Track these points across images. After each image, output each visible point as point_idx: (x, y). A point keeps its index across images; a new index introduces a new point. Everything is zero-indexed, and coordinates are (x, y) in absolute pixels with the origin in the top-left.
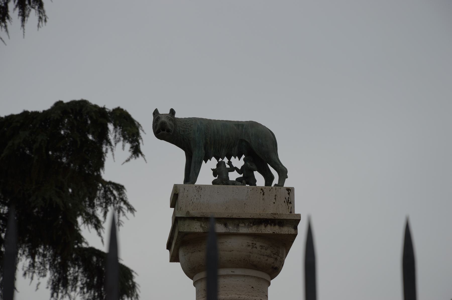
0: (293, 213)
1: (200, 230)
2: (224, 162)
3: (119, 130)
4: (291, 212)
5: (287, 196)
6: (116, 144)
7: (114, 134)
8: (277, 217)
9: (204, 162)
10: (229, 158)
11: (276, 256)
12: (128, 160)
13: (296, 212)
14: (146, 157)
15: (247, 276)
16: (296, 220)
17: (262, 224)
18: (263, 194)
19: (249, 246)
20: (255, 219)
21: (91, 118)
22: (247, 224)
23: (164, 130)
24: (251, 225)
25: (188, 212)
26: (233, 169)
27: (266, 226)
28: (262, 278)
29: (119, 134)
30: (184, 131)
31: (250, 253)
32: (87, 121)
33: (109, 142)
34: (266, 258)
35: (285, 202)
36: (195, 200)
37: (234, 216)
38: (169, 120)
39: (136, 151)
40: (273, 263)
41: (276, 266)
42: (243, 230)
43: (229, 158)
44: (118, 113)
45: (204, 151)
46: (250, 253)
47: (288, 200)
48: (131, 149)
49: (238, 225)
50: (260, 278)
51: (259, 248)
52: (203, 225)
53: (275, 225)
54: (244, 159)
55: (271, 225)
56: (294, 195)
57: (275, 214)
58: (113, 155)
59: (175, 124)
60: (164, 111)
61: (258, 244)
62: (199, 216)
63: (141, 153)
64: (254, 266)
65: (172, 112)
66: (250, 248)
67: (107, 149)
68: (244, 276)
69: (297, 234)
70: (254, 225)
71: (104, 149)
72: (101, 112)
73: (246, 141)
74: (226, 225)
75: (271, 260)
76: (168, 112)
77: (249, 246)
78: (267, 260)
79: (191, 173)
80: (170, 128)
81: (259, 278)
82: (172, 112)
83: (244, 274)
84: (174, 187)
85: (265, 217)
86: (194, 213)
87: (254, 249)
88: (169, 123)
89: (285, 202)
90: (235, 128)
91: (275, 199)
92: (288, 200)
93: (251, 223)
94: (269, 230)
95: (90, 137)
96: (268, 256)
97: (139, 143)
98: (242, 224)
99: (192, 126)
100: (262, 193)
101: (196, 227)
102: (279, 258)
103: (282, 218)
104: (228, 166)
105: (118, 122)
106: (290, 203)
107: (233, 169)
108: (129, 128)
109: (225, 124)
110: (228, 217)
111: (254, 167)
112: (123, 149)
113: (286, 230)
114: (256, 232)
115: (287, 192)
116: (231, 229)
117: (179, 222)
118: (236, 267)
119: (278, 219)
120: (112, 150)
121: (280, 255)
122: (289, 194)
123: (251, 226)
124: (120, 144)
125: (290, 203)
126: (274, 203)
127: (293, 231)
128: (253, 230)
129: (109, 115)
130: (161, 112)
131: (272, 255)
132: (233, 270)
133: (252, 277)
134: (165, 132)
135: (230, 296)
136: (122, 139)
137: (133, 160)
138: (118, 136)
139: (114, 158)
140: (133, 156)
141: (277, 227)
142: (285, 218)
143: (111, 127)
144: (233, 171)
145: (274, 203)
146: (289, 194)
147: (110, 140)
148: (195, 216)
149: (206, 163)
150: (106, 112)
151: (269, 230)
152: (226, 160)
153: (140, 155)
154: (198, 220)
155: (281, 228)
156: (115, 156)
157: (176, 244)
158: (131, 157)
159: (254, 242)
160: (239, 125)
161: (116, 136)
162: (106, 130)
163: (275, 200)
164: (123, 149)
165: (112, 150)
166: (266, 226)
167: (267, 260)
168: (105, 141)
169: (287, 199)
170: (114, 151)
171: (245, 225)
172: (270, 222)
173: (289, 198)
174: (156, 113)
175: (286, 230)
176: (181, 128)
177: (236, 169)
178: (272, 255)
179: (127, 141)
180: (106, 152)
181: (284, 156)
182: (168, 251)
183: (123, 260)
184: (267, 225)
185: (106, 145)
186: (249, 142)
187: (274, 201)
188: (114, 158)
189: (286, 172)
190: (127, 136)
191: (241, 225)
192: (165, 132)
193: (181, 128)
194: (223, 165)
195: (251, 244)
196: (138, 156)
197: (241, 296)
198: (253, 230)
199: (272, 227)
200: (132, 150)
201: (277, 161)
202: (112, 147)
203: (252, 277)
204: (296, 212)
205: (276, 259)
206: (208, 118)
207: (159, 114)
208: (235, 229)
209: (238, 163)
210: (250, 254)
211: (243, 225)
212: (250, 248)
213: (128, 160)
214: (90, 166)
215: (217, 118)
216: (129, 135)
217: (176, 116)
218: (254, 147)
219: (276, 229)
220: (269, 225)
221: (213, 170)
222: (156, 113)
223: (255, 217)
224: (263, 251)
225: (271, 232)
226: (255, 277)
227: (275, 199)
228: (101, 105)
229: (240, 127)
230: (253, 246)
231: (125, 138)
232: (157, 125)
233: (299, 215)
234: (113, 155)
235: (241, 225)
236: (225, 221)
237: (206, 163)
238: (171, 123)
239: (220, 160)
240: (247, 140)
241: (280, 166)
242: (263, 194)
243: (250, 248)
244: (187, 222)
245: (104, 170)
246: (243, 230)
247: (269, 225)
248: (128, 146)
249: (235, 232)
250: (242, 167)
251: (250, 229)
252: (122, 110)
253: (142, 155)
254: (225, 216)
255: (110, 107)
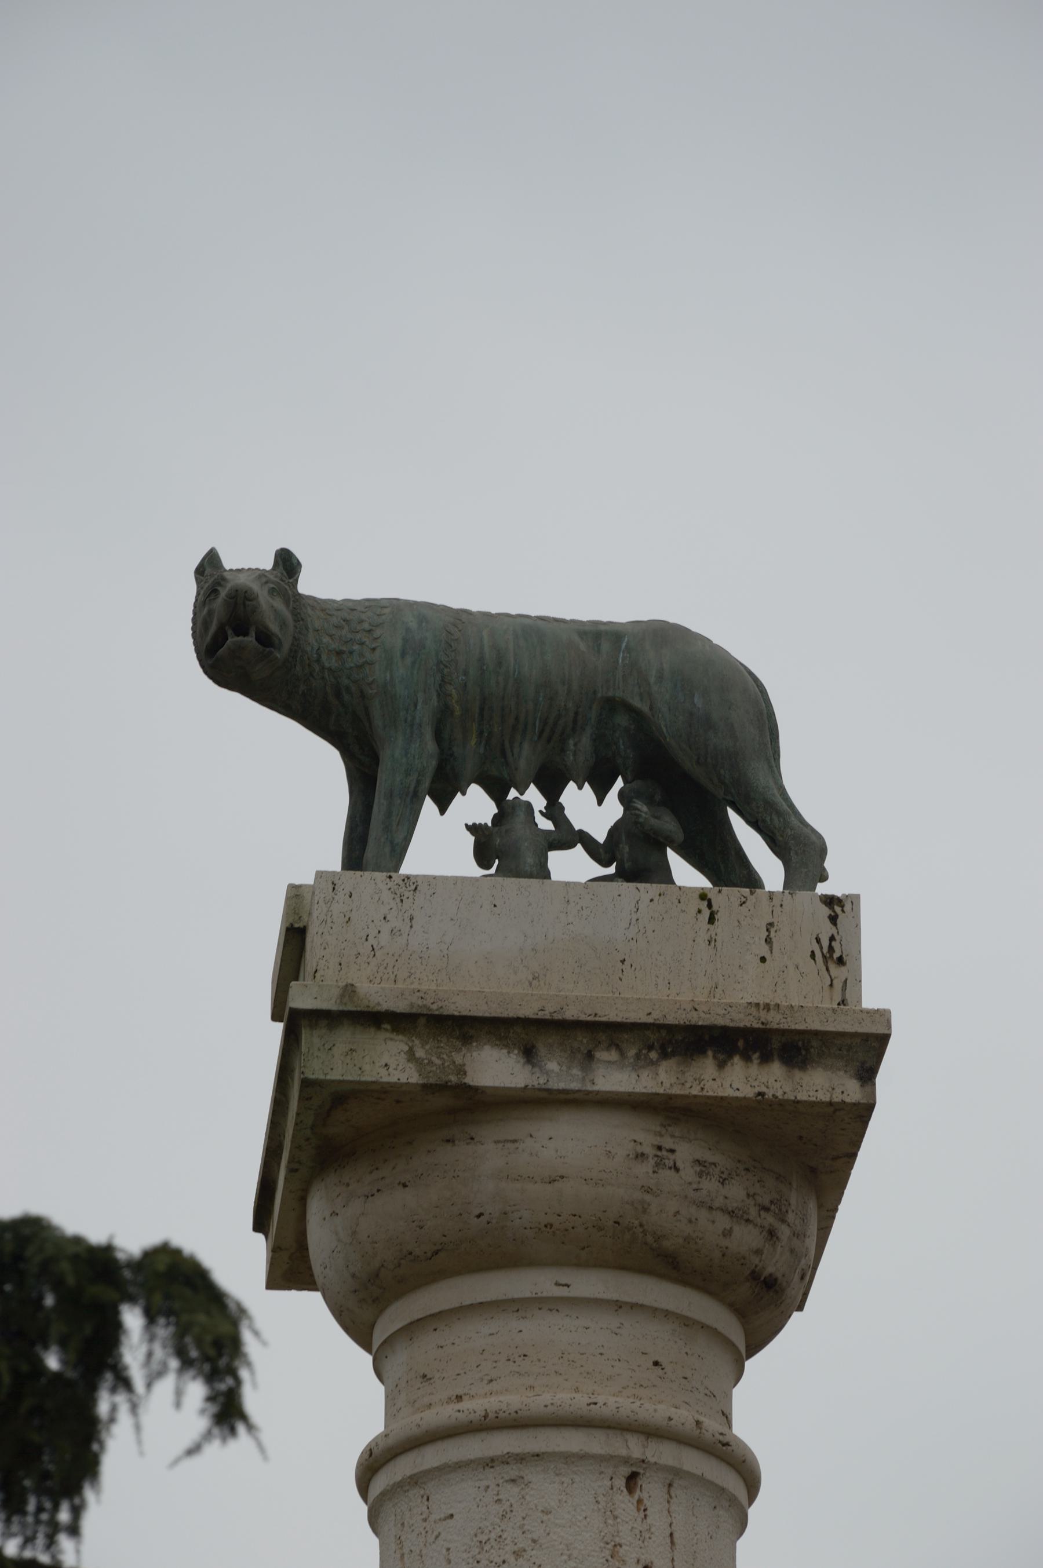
0: (851, 1006)
1: (406, 1074)
2: (529, 806)
3: (163, 1331)
4: (843, 1002)
5: (826, 930)
6: (149, 1385)
7: (143, 1349)
8: (775, 1020)
9: (429, 806)
10: (552, 793)
11: (769, 1219)
12: (194, 1450)
13: (870, 1000)
14: (265, 1436)
15: (633, 1306)
16: (866, 1037)
17: (702, 1052)
18: (712, 920)
19: (641, 1156)
20: (670, 1028)
21: (58, 1286)
22: (632, 1052)
23: (241, 630)
24: (653, 1055)
25: (349, 990)
26: (567, 837)
27: (721, 1065)
28: (703, 1326)
29: (164, 1347)
30: (339, 653)
31: (648, 1190)
32: (41, 1298)
33: (124, 1382)
34: (723, 1222)
35: (813, 955)
36: (385, 937)
37: (571, 1013)
38: (272, 592)
39: (228, 1413)
40: (758, 1252)
41: (770, 1270)
42: (614, 1077)
43: (552, 793)
44: (161, 1266)
45: (431, 746)
46: (648, 1190)
47: (831, 949)
48: (208, 1405)
49: (590, 1056)
50: (695, 1322)
51: (688, 1173)
52: (420, 1053)
53: (766, 1059)
54: (622, 796)
55: (747, 1058)
56: (858, 926)
57: (767, 1007)
58: (138, 1428)
59: (297, 616)
60: (247, 555)
61: (686, 1152)
62: (400, 1006)
63: (243, 1417)
64: (670, 1263)
65: (287, 564)
66: (647, 1167)
67: (114, 1409)
68: (618, 1306)
69: (870, 1107)
70: (665, 1055)
71: (103, 1408)
72: (100, 1261)
73: (629, 709)
74: (529, 1054)
75: (746, 1238)
76: (267, 563)
77: (641, 1156)
78: (727, 1233)
79: (373, 836)
80: (274, 627)
81: (687, 1322)
82: (287, 564)
83: (615, 1296)
84: (288, 899)
85: (720, 1022)
86: (379, 993)
87: (667, 1174)
88: (269, 607)
89: (813, 955)
90: (582, 646)
91: (768, 941)
92: (831, 949)
93: (650, 1048)
94: (738, 1080)
95: (53, 1362)
96: (731, 1214)
97: (238, 1382)
98: (608, 1049)
99: (378, 632)
100: (706, 913)
101: (389, 1062)
102: (784, 1232)
103: (802, 1027)
104: (545, 824)
105: (158, 1298)
106: (841, 961)
107: (567, 837)
108: (201, 1318)
109: (535, 631)
110: (541, 1015)
111: (668, 824)
112: (178, 1404)
113: (821, 1084)
114: (676, 1090)
115: (825, 911)
116: (557, 1072)
117: (305, 1035)
118: (580, 1264)
119: (783, 1032)
120: (134, 1408)
121: (791, 1217)
122: (833, 919)
123: (652, 1063)
124: (166, 1385)
125: (841, 961)
126: (763, 960)
127: (851, 1091)
128: (662, 1079)
129: (127, 1274)
130: (230, 562)
131: (753, 1212)
132: (565, 1275)
133: (654, 1312)
134: (250, 639)
135: (546, 1398)
136: (174, 1363)
137: (214, 1449)
138: (159, 1353)
139: (139, 1442)
140: (216, 1431)
141: (776, 1069)
142: (815, 1025)
143: (132, 1319)
144: (570, 846)
145: (763, 960)
146: (833, 919)
147: (125, 1368)
148: (384, 1007)
149: (443, 811)
150: (115, 1261)
151: (738, 1080)
152: (534, 797)
153: (241, 1428)
154: (396, 1030)
155: (798, 1074)
156: (146, 1434)
157: (291, 1170)
158: (208, 1436)
159: (668, 1143)
160: (599, 635)
161: (150, 1355)
162: (111, 1333)
163: (766, 947)
164: (178, 1404)
165: (134, 1408)
166: (721, 1065)
167: (727, 1233)
168: (109, 1376)
169: (825, 943)
170: (141, 1410)
171: (623, 1054)
172: (741, 1043)
173: (832, 938)
174: (209, 568)
175: (821, 1084)
176: (326, 640)
177: (584, 839)
178: (753, 1212)
179: (191, 1373)
180: (112, 1420)
181: (808, 777)
182: (261, 1237)
183: (98, 1501)
184: (730, 1056)
185: (113, 1390)
186: (645, 708)
187: (764, 950)
188: (139, 1442)
189: (821, 850)
190: (194, 1353)
191: (602, 1055)
192: (250, 639)
193: (326, 640)
194: (521, 816)
195: (649, 1150)
196: (233, 1431)
197: (600, 1400)
198: (662, 1079)
199: (754, 1069)
200: (213, 1409)
201: (779, 799)
202: (135, 1399)
203: (654, 1312)
204: (870, 1000)
205: (772, 1234)
206: (456, 603)
207: (225, 570)
208: (576, 1071)
209: (592, 811)
210: (648, 1197)
211: (613, 1055)
212: (647, 1167)
213: (194, 1450)
214: (46, 1476)
215: (494, 607)
216: (199, 1343)
217: (307, 585)
218: (666, 746)
219: (773, 1080)
220: (737, 1059)
221: (473, 829)
222: (209, 568)
223: (671, 1020)
224: (710, 1185)
225: (747, 1092)
226: (667, 1314)
227: (768, 941)
228: (96, 1236)
229: (606, 647)
230: (663, 1158)
231: (186, 1363)
232: (210, 613)
233: (883, 1016)
234: (138, 1428)
235: (602, 1055)
236: (524, 1033)
237: (443, 811)
238: (278, 604)
239: (513, 794)
240: (636, 703)
241: (793, 820)
242: (712, 920)
243: (643, 1169)
244: (344, 1038)
245: (98, 1492)
246: (614, 1077)
247: (737, 1059)
248: (196, 1391)
249: (574, 1086)
250: (613, 832)
251: (645, 1074)
252: (177, 1253)
253: (250, 1427)
254: (528, 1011)
255: (132, 1242)
